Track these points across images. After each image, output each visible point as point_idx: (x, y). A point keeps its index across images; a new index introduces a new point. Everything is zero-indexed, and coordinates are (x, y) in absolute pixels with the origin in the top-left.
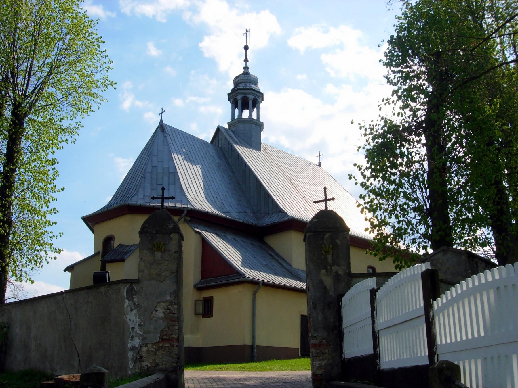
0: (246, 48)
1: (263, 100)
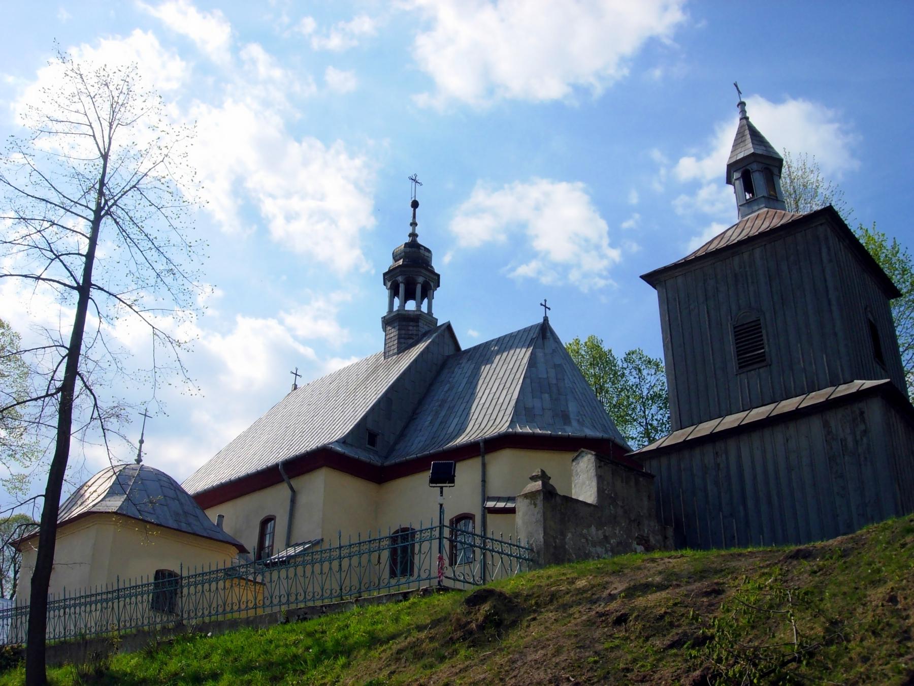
0: (415, 205)
1: (439, 286)
